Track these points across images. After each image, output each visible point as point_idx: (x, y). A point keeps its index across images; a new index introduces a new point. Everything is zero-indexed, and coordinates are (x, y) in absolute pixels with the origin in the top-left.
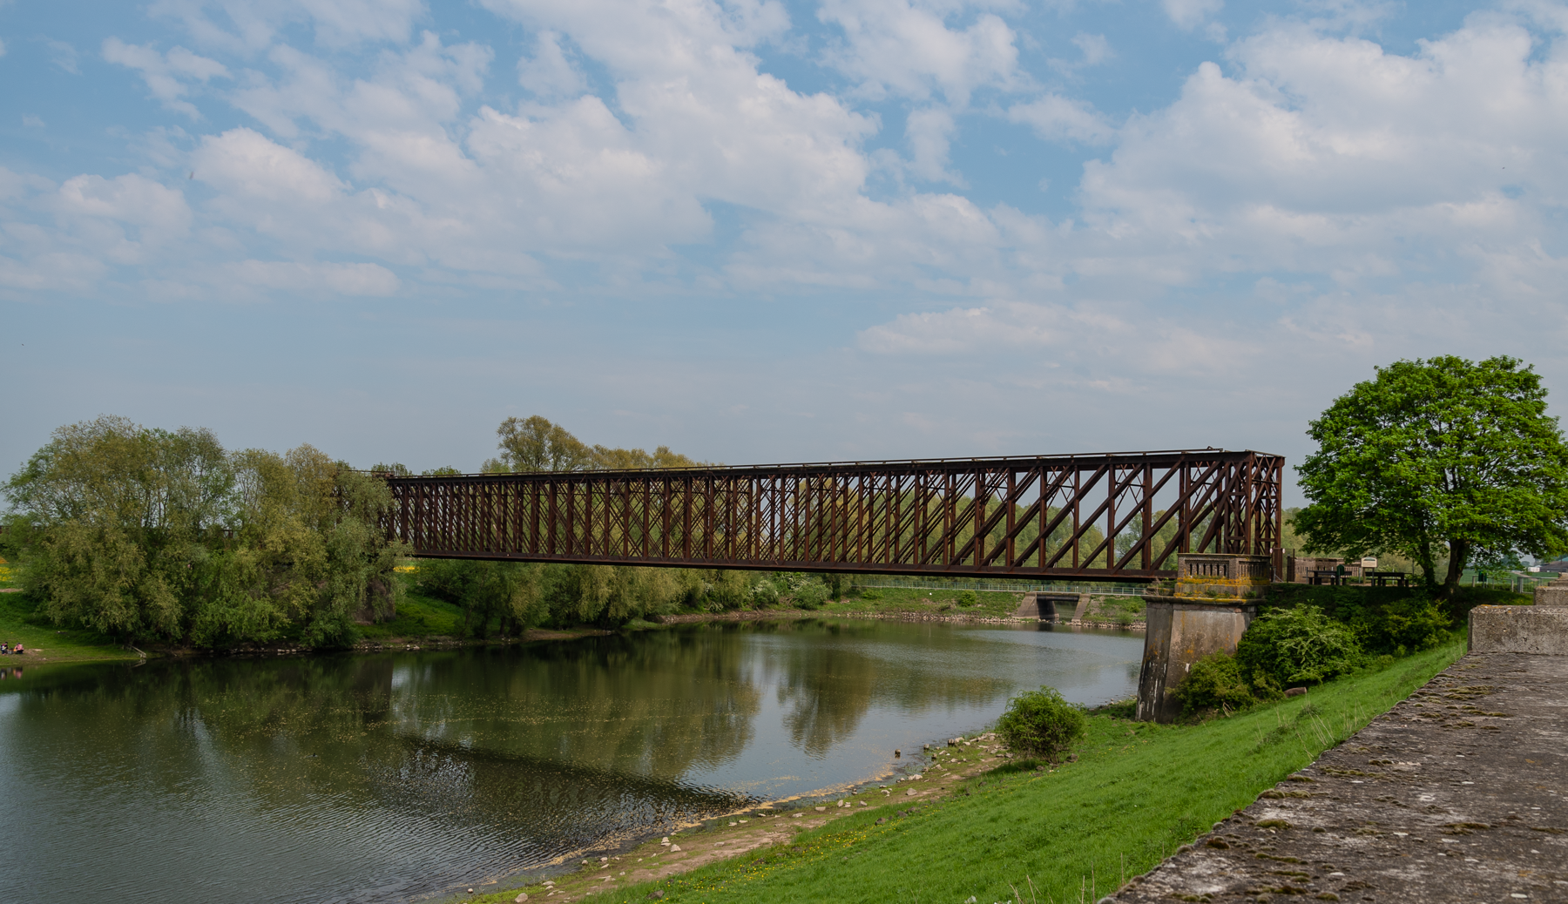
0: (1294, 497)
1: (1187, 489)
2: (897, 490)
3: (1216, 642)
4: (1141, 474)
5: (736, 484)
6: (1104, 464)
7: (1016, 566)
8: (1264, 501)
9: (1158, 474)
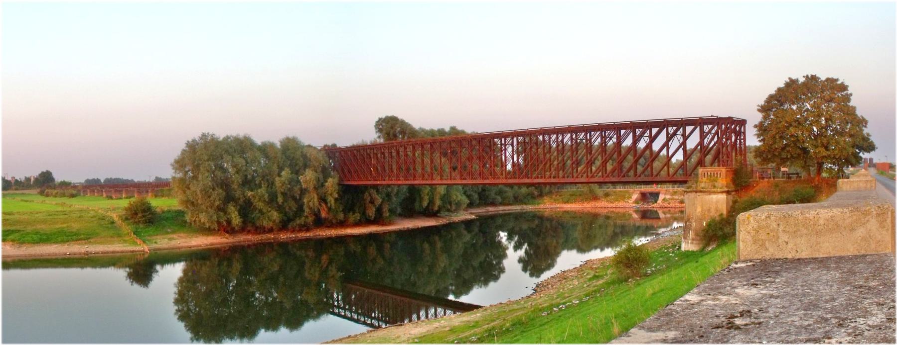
0: (752, 140)
1: (703, 136)
2: (562, 141)
3: (717, 211)
5: (505, 140)
6: (663, 124)
7: (622, 177)
8: (738, 141)
9: (689, 129)
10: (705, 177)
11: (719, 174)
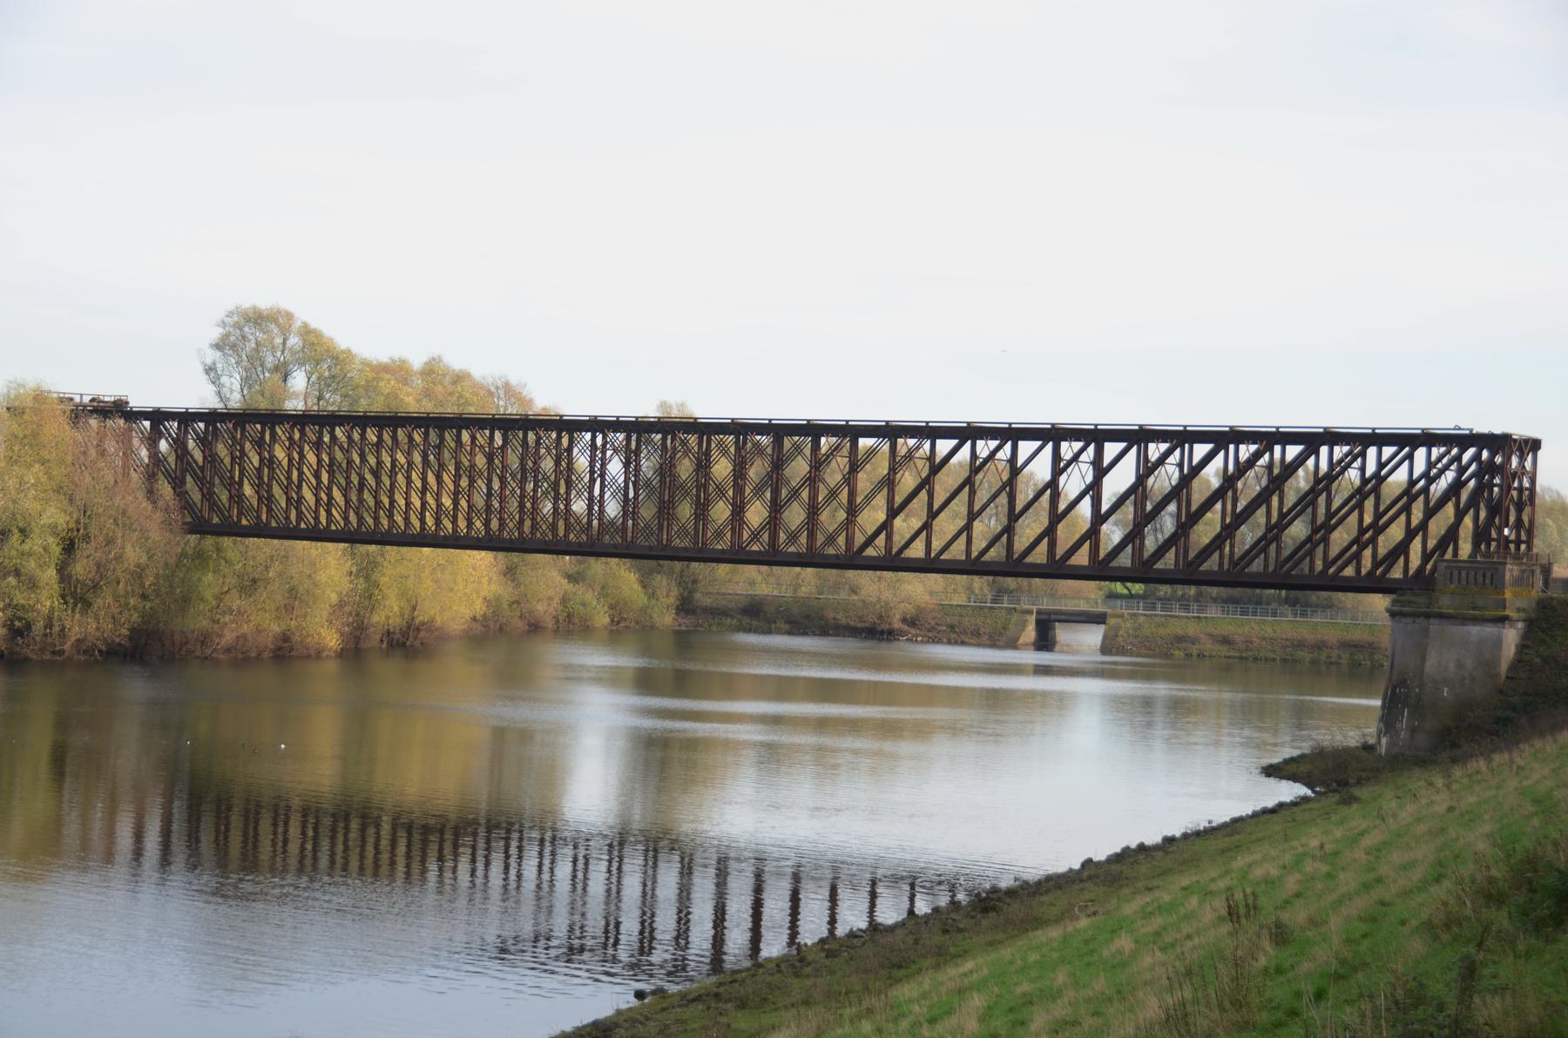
1: (1147, 469)
4: (1091, 448)
10: (1451, 582)
11: (1488, 575)
